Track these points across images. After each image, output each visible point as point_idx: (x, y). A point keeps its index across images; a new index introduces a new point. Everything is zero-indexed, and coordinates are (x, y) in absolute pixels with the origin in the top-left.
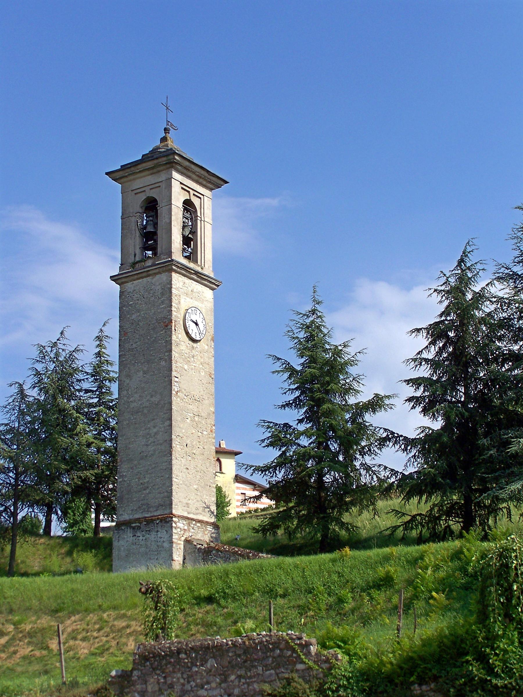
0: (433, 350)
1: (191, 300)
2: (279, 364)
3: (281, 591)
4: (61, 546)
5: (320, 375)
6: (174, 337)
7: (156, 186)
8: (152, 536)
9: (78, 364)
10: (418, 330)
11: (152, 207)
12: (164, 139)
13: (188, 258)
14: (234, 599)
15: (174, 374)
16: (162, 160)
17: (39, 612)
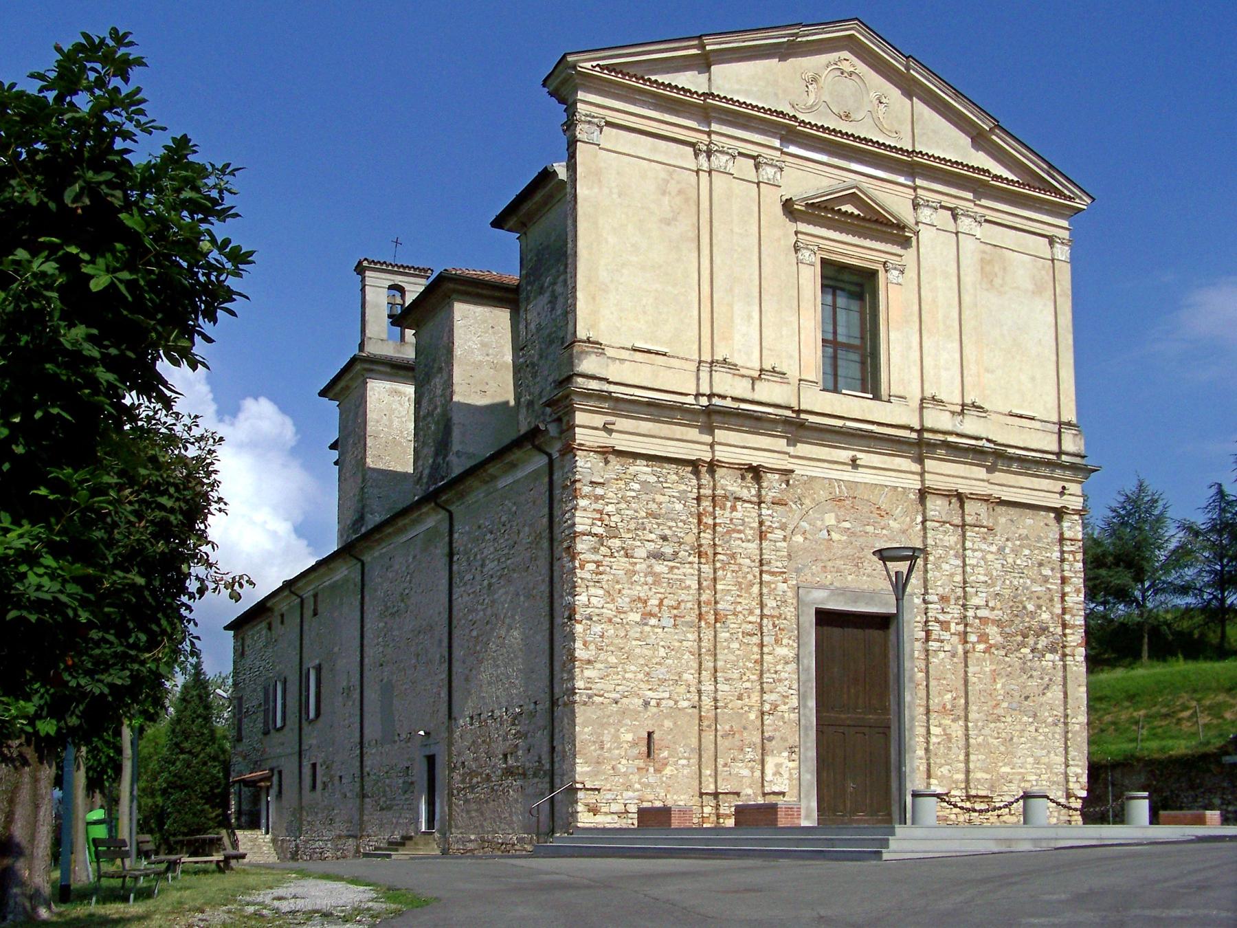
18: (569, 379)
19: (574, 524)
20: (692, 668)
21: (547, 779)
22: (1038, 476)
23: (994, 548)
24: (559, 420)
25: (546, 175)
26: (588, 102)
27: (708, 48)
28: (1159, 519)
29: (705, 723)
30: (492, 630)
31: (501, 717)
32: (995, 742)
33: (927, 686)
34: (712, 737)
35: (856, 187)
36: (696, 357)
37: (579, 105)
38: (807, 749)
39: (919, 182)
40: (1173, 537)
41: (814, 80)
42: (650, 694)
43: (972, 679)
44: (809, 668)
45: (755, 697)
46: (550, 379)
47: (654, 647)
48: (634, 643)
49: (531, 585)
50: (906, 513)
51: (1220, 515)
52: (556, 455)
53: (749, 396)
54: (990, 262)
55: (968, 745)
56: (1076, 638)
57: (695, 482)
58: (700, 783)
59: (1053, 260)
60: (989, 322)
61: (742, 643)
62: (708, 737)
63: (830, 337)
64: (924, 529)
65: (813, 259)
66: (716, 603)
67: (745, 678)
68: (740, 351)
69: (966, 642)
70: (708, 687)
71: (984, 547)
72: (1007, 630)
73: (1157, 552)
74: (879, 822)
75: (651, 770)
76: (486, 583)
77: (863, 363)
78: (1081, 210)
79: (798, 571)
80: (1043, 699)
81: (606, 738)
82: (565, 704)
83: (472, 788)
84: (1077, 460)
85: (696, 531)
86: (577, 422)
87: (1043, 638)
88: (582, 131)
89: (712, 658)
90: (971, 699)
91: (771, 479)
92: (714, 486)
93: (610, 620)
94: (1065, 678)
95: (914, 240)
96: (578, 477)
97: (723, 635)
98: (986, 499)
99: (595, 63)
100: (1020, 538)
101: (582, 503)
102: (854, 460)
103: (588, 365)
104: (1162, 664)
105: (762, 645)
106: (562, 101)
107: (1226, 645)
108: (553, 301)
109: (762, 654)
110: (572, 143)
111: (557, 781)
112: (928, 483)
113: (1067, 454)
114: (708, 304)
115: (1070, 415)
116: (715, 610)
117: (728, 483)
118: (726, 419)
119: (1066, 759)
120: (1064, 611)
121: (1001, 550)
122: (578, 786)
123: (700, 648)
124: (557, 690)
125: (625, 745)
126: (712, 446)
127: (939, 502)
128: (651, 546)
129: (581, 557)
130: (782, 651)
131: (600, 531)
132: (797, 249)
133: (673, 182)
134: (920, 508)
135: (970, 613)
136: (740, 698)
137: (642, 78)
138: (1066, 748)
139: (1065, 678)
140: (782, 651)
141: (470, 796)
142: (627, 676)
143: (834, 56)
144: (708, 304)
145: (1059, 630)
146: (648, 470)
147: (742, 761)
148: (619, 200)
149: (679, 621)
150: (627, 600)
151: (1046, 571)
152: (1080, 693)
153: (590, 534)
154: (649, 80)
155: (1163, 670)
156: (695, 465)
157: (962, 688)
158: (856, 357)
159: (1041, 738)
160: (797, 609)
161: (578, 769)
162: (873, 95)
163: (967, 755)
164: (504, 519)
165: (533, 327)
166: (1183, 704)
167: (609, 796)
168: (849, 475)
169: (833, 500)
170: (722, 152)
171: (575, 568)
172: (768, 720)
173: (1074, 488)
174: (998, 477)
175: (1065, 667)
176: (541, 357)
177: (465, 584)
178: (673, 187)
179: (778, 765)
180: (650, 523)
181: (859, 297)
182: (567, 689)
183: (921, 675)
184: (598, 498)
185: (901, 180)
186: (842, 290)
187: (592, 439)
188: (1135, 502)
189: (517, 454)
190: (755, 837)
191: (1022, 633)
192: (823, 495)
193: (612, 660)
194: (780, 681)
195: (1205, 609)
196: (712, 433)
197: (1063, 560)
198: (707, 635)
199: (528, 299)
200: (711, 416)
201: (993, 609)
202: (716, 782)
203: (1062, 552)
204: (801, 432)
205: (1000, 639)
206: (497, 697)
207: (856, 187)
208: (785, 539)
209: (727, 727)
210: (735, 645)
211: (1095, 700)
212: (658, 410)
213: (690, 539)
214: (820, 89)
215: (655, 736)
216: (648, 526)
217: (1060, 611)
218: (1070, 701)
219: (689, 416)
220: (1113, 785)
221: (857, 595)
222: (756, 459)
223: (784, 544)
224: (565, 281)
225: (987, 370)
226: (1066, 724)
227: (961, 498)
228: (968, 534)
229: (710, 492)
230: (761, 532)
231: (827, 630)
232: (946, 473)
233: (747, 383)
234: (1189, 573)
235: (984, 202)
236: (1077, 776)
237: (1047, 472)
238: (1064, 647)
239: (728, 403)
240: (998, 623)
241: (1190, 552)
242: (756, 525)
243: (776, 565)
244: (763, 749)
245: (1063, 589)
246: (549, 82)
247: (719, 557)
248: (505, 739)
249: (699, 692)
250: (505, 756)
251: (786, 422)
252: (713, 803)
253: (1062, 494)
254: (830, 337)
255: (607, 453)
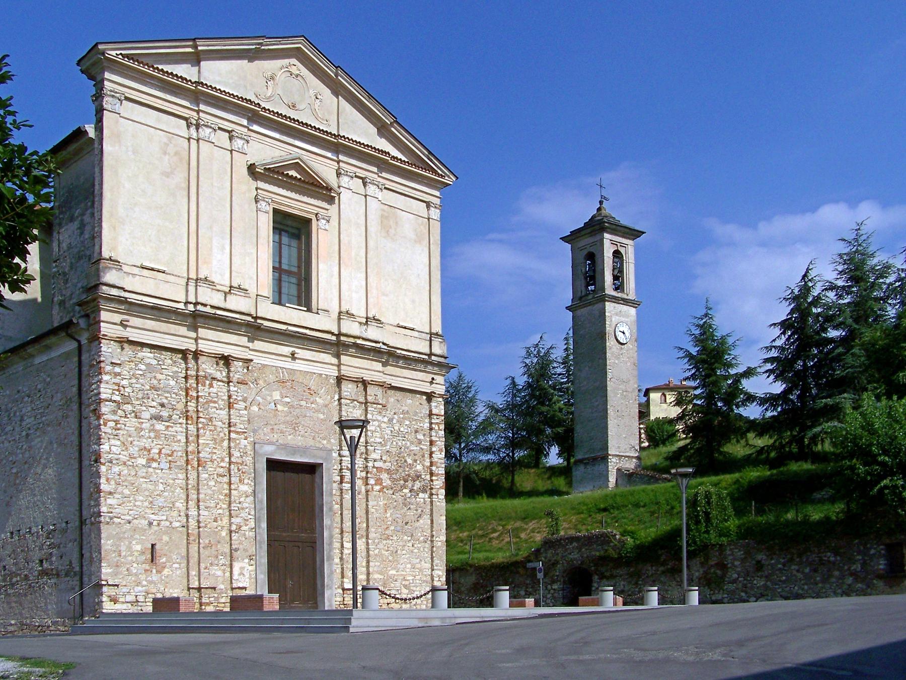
0: (784, 338)
1: (620, 320)
2: (682, 352)
3: (642, 504)
4: (545, 473)
5: (709, 356)
6: (608, 344)
7: (593, 244)
8: (596, 468)
9: (553, 357)
10: (775, 324)
11: (591, 256)
12: (599, 209)
13: (616, 289)
14: (618, 509)
15: (608, 367)
16: (597, 226)
17: (516, 519)
18: (96, 286)
19: (99, 393)
20: (181, 498)
21: (78, 578)
22: (416, 370)
23: (386, 420)
24: (87, 316)
25: (79, 133)
26: (112, 81)
27: (200, 48)
28: (472, 401)
29: (191, 538)
30: (29, 468)
31: (38, 532)
32: (386, 553)
33: (341, 514)
34: (196, 548)
35: (299, 158)
36: (185, 275)
37: (106, 83)
38: (261, 557)
39: (341, 157)
40: (481, 411)
41: (272, 78)
42: (153, 517)
43: (371, 510)
44: (261, 502)
45: (226, 520)
46: (80, 285)
47: (156, 483)
48: (142, 480)
49: (63, 436)
50: (327, 393)
51: (512, 398)
52: (84, 341)
53: (222, 306)
54: (387, 218)
55: (368, 556)
56: (439, 483)
57: (184, 365)
58: (188, 581)
59: (429, 219)
60: (386, 262)
61: (216, 482)
62: (194, 548)
63: (277, 265)
64: (340, 404)
65: (268, 208)
66: (199, 452)
67: (219, 507)
68: (216, 272)
69: (367, 484)
70: (193, 512)
71: (380, 418)
72: (394, 476)
73: (470, 423)
74: (310, 608)
75: (154, 571)
76: (24, 433)
77: (299, 285)
78: (448, 185)
79: (254, 431)
80: (417, 524)
81: (123, 548)
82: (92, 524)
83: (13, 585)
84: (442, 360)
85: (184, 401)
86: (102, 319)
87: (417, 482)
88: (108, 103)
89: (196, 492)
90: (371, 524)
91: (237, 366)
92: (198, 369)
93: (125, 464)
94: (432, 510)
95: (337, 199)
96: (102, 359)
97: (204, 476)
98: (381, 385)
99: (118, 52)
100: (403, 413)
101: (106, 378)
102: (293, 354)
103: (110, 277)
104: (471, 501)
105: (230, 484)
106: (91, 78)
107: (515, 488)
108: (82, 226)
109: (230, 490)
110: (100, 111)
111: (86, 579)
112: (343, 372)
113: (435, 355)
114: (194, 234)
115: (437, 328)
116: (198, 458)
117: (208, 367)
118: (207, 321)
119: (432, 565)
120: (432, 464)
121: (391, 420)
122: (103, 583)
123: (187, 484)
124: (85, 513)
125: (136, 554)
126: (196, 340)
127: (350, 386)
128: (153, 411)
129: (105, 417)
130: (244, 488)
131: (118, 398)
132: (257, 201)
133: (172, 145)
134: (337, 390)
135: (370, 464)
136: (215, 520)
137: (153, 67)
138: (432, 558)
139: (432, 510)
140: (244, 488)
141: (10, 591)
142: (137, 503)
143: (286, 62)
144: (194, 234)
145: (428, 477)
146: (152, 355)
147: (217, 565)
148: (133, 156)
149: (173, 465)
150: (137, 449)
151: (420, 437)
152: (442, 520)
153: (110, 400)
154: (157, 68)
155: (472, 505)
156: (184, 353)
157: (365, 516)
158: (294, 280)
159: (416, 551)
160: (254, 458)
161: (103, 570)
162: (312, 93)
163: (368, 562)
164: (39, 387)
165: (64, 246)
166: (493, 528)
167: (125, 590)
168: (289, 365)
169: (278, 381)
170: (207, 126)
171: (100, 425)
172: (235, 536)
173: (440, 379)
174: (389, 369)
175: (432, 502)
176: (71, 268)
177: (6, 434)
178: (171, 149)
179: (242, 568)
180: (153, 394)
181: (296, 236)
182: (94, 513)
183: (337, 507)
184: (117, 374)
185: (329, 155)
186: (286, 231)
187: (112, 331)
188: (456, 387)
189: (53, 340)
190: (245, 618)
191: (404, 478)
192: (272, 378)
193: (127, 492)
194: (243, 509)
195: (500, 463)
196: (196, 331)
197: (431, 429)
198: (193, 475)
199: (60, 224)
200: (197, 318)
201: (385, 462)
202: (199, 580)
203: (431, 423)
204: (259, 333)
205: (389, 482)
206: (34, 518)
207: (299, 158)
208: (246, 408)
209: (207, 541)
210: (212, 483)
211: (453, 523)
212: (159, 312)
213: (180, 406)
214: (276, 85)
215: (157, 547)
216: (151, 396)
217: (429, 464)
218: (435, 525)
219: (180, 318)
220: (453, 583)
221: (295, 450)
222: (227, 351)
223: (246, 412)
224: (93, 214)
225: (384, 294)
226: (432, 541)
227: (365, 383)
228: (369, 409)
229: (195, 373)
230: (230, 403)
231: (273, 473)
232: (354, 365)
233: (221, 296)
234: (491, 438)
235: (384, 175)
236: (439, 576)
237: (422, 367)
238: (432, 489)
239: (208, 309)
240: (388, 471)
241: (491, 424)
242: (226, 398)
243: (240, 427)
244: (231, 557)
245: (431, 449)
246: (83, 62)
247: (201, 420)
248: (41, 549)
249: (187, 516)
250: (41, 561)
251: (248, 325)
252: (197, 595)
253: (431, 383)
254: (277, 265)
255: (123, 342)
